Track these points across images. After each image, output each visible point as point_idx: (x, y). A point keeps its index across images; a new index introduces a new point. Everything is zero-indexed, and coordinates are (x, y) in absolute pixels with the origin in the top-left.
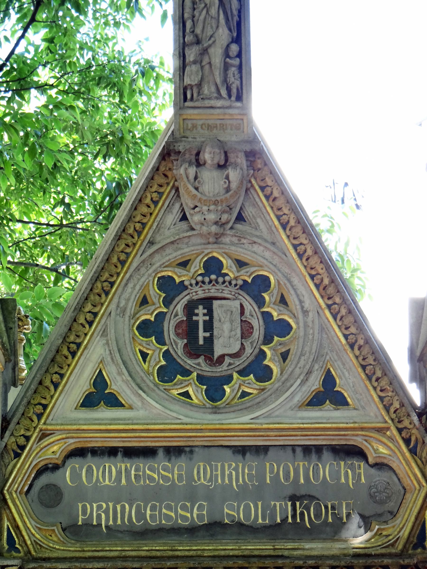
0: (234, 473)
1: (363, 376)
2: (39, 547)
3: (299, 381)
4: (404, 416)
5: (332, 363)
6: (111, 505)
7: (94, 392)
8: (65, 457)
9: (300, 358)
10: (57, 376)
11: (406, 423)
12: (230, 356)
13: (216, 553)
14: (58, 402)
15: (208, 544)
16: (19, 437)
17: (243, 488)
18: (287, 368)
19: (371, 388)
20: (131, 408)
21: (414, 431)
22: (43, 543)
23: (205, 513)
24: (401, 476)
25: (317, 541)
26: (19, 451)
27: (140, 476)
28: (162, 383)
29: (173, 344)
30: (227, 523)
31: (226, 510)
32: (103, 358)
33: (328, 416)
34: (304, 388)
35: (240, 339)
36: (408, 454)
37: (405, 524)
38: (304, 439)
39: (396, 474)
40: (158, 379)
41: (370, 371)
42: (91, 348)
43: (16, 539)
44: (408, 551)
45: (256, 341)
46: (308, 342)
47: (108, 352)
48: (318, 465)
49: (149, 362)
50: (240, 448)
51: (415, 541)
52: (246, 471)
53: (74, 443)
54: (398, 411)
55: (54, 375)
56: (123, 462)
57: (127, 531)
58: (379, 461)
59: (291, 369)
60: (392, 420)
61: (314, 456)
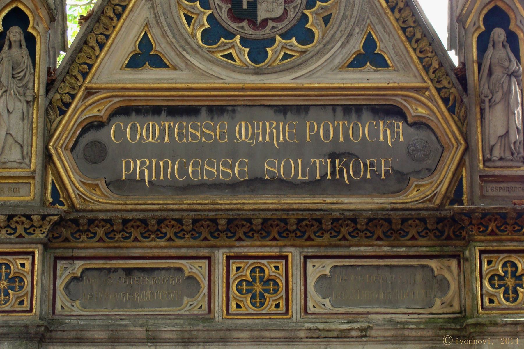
0: (275, 131)
1: (403, 38)
2: (83, 200)
3: (340, 43)
4: (443, 75)
5: (372, 27)
6: (154, 162)
7: (140, 54)
8: (110, 115)
9: (341, 22)
10: (103, 37)
11: (445, 83)
12: (274, 20)
13: (256, 206)
14: (103, 63)
15: (250, 198)
16: (65, 95)
17: (284, 145)
18: (328, 31)
19: (411, 50)
20: (175, 68)
21: (453, 90)
22: (87, 197)
23: (246, 169)
24: (439, 134)
25: (355, 196)
26: (64, 108)
27: (183, 133)
28: (206, 46)
29: (218, 8)
30: (267, 179)
31: (267, 167)
32: (148, 21)
33: (369, 78)
34: (345, 51)
35: (283, 3)
36: (446, 113)
37: (442, 180)
38: (344, 99)
39: (434, 133)
40: (202, 42)
41: (410, 32)
42: (137, 11)
43: (60, 193)
44: (445, 206)
45: (299, 6)
46: (349, 7)
47: (153, 15)
48: (357, 124)
49: (194, 25)
50: (281, 108)
51: (452, 196)
52: (287, 129)
53: (119, 101)
54: (437, 71)
55: (100, 36)
56: (167, 121)
57: (170, 186)
58: (416, 119)
59: (332, 32)
60: (431, 80)
61: (354, 115)
